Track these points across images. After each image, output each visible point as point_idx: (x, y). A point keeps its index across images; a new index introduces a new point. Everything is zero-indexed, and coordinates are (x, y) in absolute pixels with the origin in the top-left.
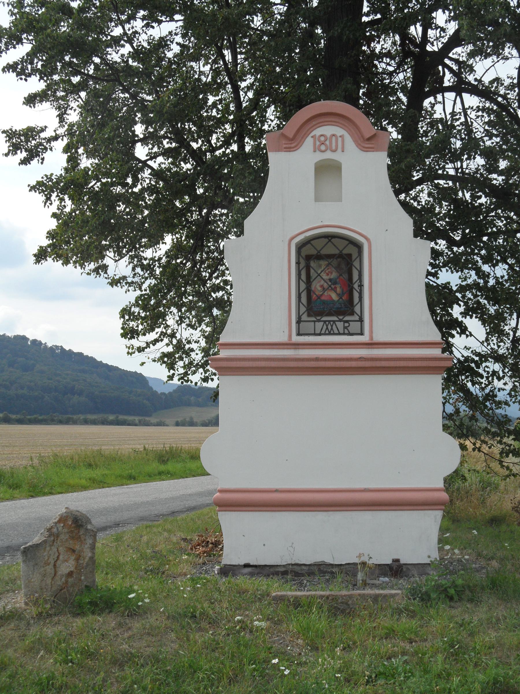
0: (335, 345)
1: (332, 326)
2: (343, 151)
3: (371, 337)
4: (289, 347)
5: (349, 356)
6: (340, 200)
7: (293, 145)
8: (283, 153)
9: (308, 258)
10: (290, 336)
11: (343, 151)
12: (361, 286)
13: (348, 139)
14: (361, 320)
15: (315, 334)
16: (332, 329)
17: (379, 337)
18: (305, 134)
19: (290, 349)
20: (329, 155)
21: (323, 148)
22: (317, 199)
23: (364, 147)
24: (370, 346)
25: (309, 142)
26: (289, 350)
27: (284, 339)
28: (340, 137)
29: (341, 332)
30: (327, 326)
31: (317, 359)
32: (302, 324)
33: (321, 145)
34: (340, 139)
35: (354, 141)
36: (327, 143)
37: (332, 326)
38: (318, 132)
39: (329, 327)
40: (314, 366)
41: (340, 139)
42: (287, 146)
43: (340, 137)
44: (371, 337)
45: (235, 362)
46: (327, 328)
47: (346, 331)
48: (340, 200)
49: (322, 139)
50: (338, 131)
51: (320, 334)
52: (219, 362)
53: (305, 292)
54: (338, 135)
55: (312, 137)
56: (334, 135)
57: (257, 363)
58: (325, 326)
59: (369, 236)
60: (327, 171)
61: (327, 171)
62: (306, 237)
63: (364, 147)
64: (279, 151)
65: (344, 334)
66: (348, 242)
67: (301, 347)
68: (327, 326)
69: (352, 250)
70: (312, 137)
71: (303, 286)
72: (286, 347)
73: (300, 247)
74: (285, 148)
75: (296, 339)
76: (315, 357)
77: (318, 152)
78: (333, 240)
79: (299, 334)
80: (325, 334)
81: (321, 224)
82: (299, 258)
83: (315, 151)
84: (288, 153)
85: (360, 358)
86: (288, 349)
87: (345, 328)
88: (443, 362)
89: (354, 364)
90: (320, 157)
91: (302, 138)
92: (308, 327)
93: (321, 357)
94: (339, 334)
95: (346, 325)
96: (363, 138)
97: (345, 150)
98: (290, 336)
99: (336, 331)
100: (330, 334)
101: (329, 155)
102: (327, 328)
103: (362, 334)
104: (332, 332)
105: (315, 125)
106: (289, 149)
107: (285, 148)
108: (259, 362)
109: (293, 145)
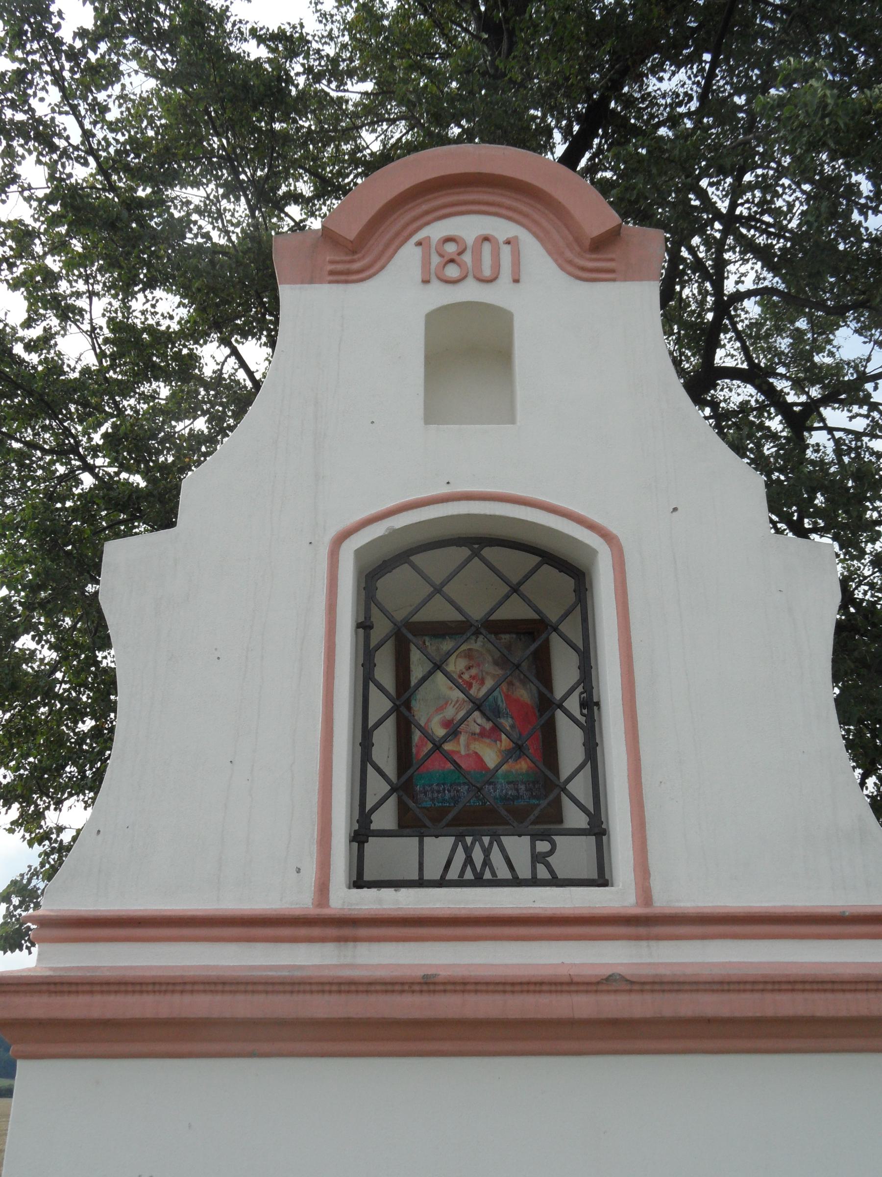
0: (490, 930)
1: (487, 852)
2: (516, 281)
3: (645, 894)
4: (316, 931)
5: (563, 972)
6: (513, 421)
7: (356, 266)
8: (326, 287)
9: (406, 636)
10: (323, 889)
11: (516, 281)
12: (591, 705)
13: (533, 251)
14: (598, 829)
15: (421, 883)
16: (487, 862)
17: (678, 893)
18: (397, 234)
19: (323, 940)
20: (470, 292)
21: (452, 271)
22: (432, 415)
23: (583, 269)
24: (642, 930)
25: (408, 257)
26: (316, 947)
27: (297, 898)
28: (508, 242)
29: (524, 872)
30: (468, 851)
31: (428, 984)
32: (373, 845)
33: (448, 263)
34: (506, 252)
35: (550, 253)
36: (467, 258)
37: (487, 852)
38: (436, 231)
39: (478, 856)
40: (417, 1014)
41: (506, 252)
42: (340, 267)
43: (508, 242)
44: (645, 894)
45: (83, 999)
46: (469, 860)
47: (543, 873)
48: (513, 421)
49: (451, 248)
50: (501, 228)
51: (442, 883)
52: (16, 1000)
53: (390, 725)
54: (502, 238)
55: (419, 244)
56: (486, 239)
57: (176, 999)
58: (460, 849)
59: (613, 528)
60: (469, 355)
61: (469, 355)
62: (393, 533)
63: (583, 269)
64: (312, 281)
65: (534, 882)
66: (538, 559)
67: (363, 932)
68: (468, 851)
69: (549, 593)
70: (419, 244)
71: (380, 705)
72: (303, 931)
73: (373, 575)
74: (332, 273)
75: (345, 899)
76: (420, 973)
77: (435, 284)
78: (487, 552)
79: (359, 882)
80: (460, 883)
81: (445, 490)
82: (367, 610)
83: (426, 282)
84: (341, 287)
85: (609, 979)
86: (311, 940)
87: (537, 858)
88: (799, 997)
89: (583, 1006)
90: (441, 296)
91: (387, 246)
92: (395, 853)
93: (443, 974)
94: (516, 882)
95: (543, 846)
96: (577, 240)
97: (523, 278)
98: (323, 889)
99: (504, 873)
100: (479, 881)
101: (470, 292)
102: (469, 860)
103: (602, 880)
104: (488, 875)
105: (427, 213)
106: (343, 276)
107: (332, 273)
108: (187, 999)
109: (356, 266)
